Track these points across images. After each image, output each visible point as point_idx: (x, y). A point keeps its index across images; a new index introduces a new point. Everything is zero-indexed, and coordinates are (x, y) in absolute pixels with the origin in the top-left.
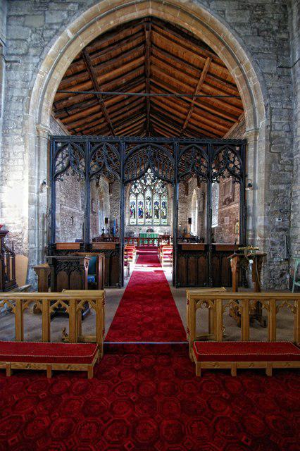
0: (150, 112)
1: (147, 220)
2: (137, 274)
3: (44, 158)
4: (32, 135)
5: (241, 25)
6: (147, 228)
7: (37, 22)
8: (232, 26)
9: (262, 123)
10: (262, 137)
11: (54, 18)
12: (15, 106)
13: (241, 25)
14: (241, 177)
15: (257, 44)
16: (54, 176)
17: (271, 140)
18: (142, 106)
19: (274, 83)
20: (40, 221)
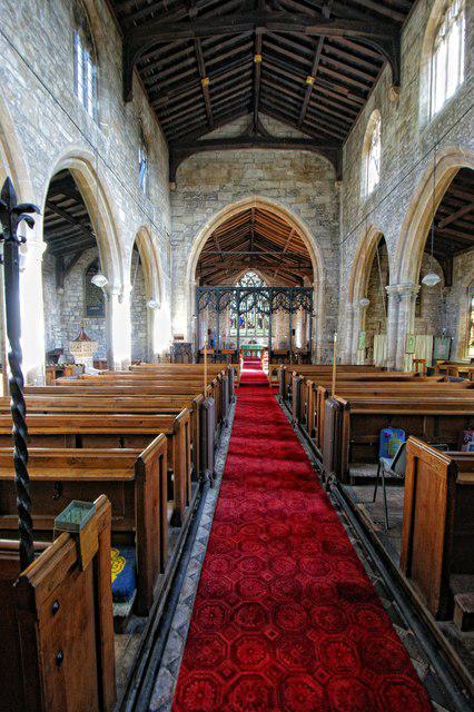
0: (262, 76)
1: (250, 330)
2: (245, 377)
3: (193, 301)
4: (188, 288)
5: (310, 219)
6: (249, 339)
7: (188, 220)
8: (304, 220)
9: (321, 279)
10: (321, 287)
11: (198, 217)
12: (179, 272)
13: (310, 219)
14: (309, 309)
15: (321, 230)
16: (199, 310)
17: (326, 289)
18: (248, 101)
19: (330, 255)
20: (155, 268)
